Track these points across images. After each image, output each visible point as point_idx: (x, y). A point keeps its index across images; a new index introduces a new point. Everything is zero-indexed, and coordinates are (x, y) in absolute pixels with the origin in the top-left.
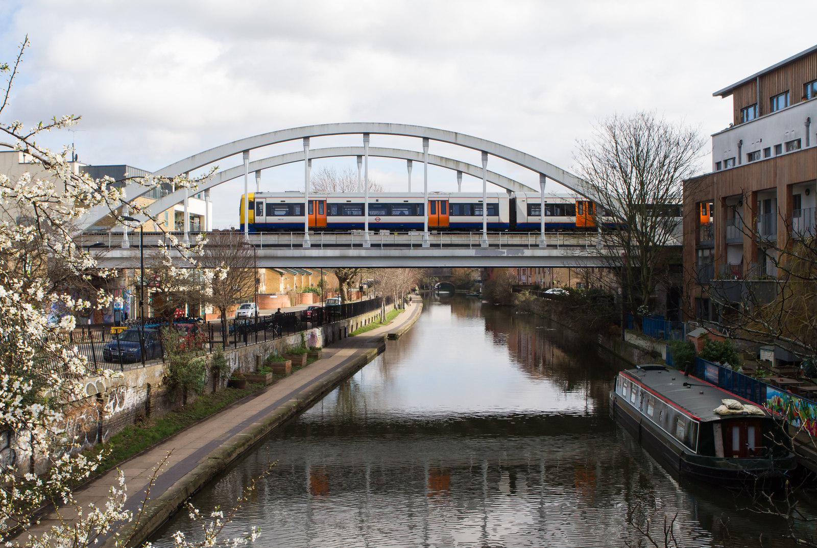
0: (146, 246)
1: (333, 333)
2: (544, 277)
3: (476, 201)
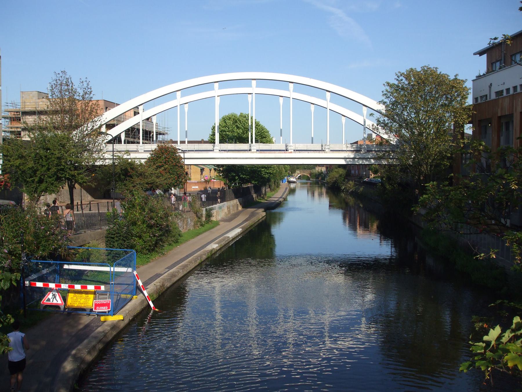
0: (98, 204)
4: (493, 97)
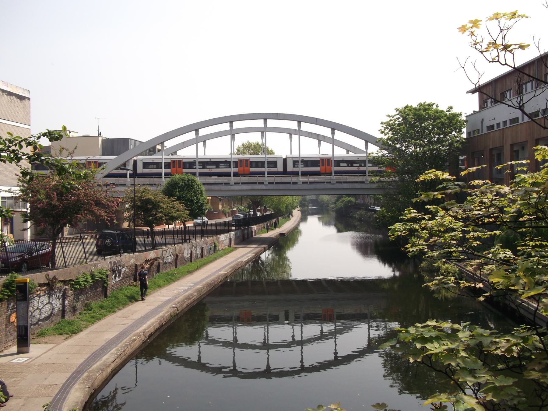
1: (248, 233)
2: (370, 200)
3: (192, 161)
4: (485, 131)
